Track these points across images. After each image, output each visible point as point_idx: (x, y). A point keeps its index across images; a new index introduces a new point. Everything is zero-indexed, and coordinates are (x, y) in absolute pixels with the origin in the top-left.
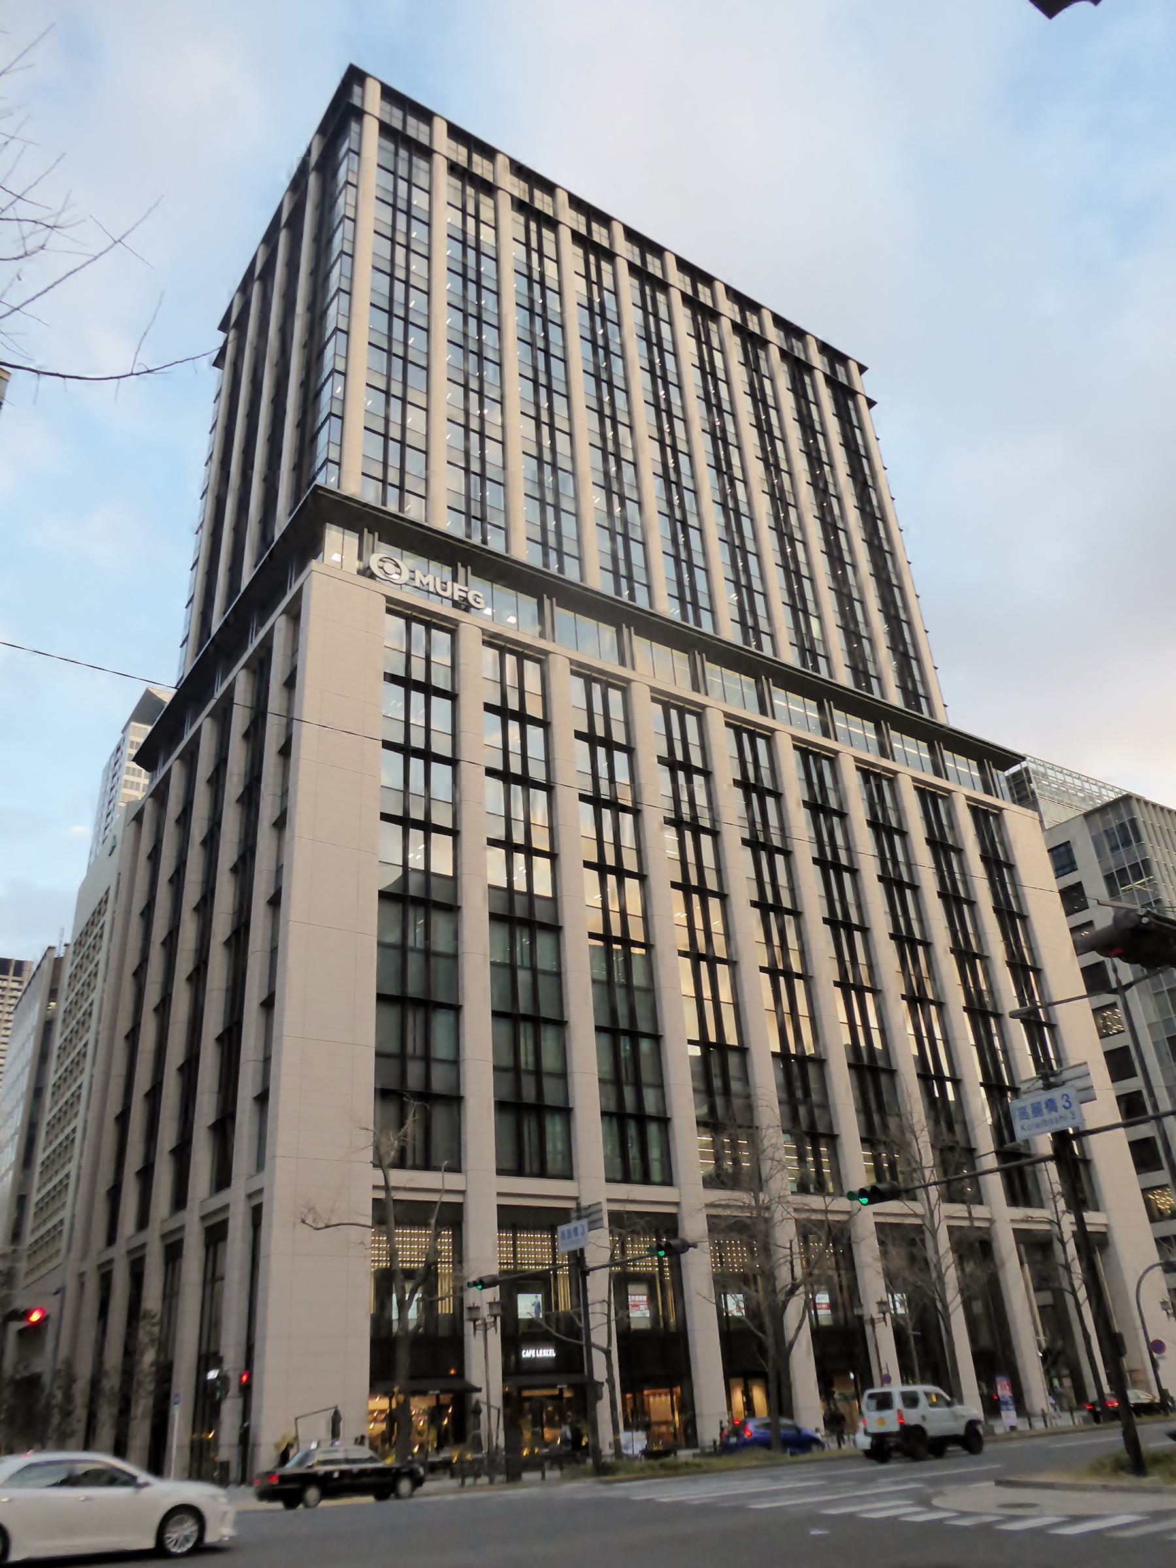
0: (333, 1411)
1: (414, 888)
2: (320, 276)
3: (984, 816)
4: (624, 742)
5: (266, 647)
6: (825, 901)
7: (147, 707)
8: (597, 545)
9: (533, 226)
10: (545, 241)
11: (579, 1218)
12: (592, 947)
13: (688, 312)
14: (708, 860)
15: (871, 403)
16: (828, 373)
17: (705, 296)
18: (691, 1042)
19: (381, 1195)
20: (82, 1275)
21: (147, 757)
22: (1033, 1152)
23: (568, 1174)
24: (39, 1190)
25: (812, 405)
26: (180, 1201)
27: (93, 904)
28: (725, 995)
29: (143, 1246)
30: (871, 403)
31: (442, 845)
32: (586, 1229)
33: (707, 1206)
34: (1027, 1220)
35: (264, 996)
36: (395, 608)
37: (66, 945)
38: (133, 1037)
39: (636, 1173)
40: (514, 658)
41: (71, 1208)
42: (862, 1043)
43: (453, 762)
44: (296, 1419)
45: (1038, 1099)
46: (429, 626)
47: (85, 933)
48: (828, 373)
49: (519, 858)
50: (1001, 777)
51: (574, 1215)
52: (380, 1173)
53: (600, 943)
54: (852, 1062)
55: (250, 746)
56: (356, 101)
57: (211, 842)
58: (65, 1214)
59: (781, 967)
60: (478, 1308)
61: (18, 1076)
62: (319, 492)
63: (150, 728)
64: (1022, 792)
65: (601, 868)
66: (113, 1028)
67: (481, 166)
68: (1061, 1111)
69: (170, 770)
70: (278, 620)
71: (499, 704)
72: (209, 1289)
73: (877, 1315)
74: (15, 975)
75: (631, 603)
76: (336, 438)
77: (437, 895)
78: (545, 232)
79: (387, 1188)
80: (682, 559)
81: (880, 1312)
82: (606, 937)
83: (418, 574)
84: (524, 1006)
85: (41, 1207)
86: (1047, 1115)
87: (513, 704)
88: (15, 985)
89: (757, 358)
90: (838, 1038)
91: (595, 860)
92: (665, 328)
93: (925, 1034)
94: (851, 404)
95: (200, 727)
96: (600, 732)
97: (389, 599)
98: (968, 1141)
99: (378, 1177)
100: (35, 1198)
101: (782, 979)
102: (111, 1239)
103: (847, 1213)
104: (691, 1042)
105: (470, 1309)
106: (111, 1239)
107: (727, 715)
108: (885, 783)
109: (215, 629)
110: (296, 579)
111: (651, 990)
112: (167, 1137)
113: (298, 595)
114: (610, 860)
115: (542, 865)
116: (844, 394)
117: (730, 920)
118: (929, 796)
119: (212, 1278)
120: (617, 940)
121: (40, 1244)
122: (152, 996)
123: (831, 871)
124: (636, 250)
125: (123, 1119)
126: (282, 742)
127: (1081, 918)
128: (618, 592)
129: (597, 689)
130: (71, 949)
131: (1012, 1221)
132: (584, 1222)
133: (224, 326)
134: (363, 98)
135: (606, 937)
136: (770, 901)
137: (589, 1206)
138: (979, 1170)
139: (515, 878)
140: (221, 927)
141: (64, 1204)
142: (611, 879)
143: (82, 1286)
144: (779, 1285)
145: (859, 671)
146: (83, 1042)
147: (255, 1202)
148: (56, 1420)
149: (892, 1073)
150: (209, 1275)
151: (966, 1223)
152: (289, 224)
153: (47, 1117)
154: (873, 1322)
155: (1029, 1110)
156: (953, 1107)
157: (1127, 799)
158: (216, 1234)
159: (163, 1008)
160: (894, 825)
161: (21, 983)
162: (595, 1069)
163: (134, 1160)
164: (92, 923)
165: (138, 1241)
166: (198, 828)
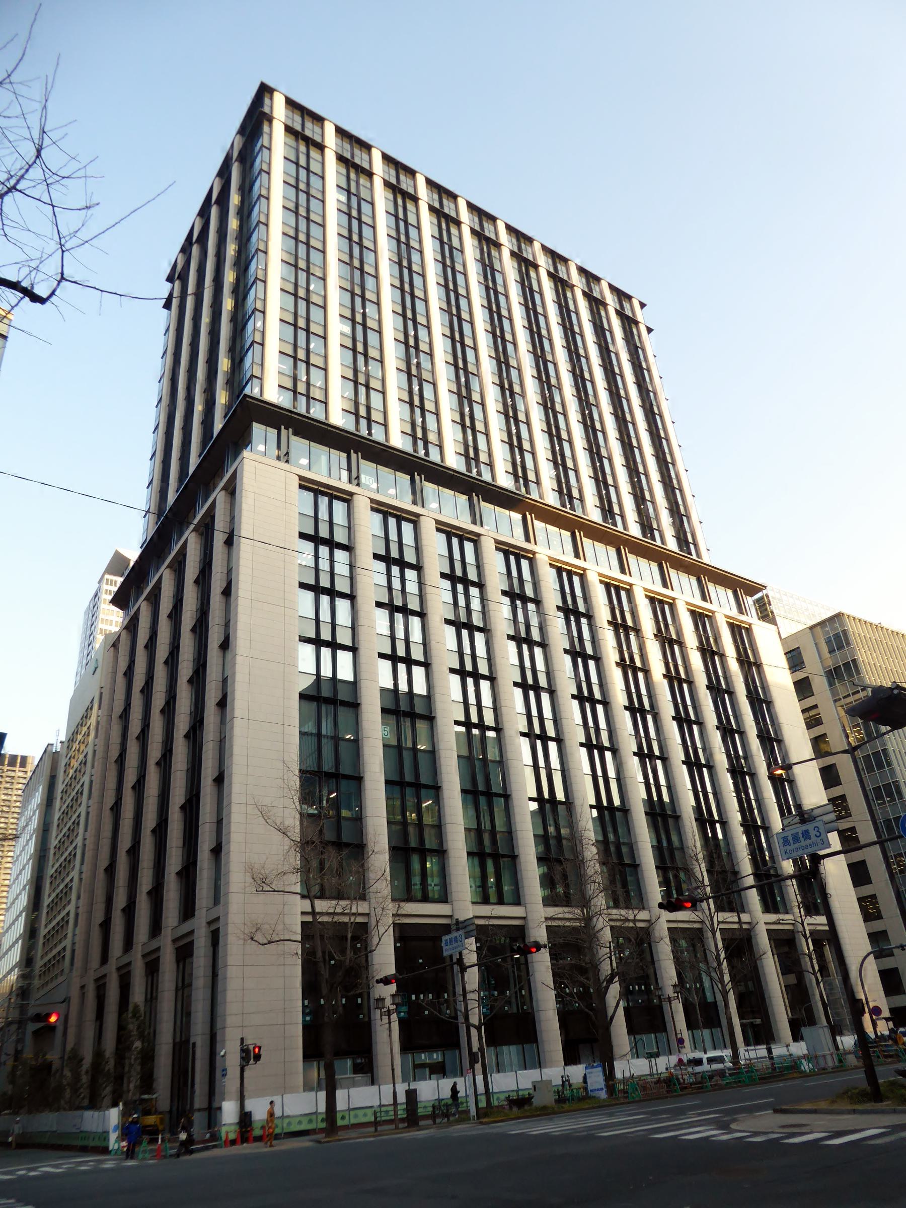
1: (326, 692)
2: (244, 237)
3: (738, 631)
4: (476, 580)
5: (210, 515)
6: (625, 693)
7: (117, 563)
8: (452, 436)
9: (353, 176)
10: (409, 214)
11: (458, 930)
12: (457, 733)
16: (618, 308)
18: (531, 799)
19: (309, 919)
20: (83, 987)
21: (120, 600)
22: (780, 873)
23: (444, 898)
24: (46, 926)
26: (156, 928)
27: (81, 711)
28: (555, 763)
29: (129, 964)
31: (345, 659)
32: (463, 937)
33: (546, 919)
34: (777, 923)
35: (216, 774)
36: (306, 484)
37: (61, 742)
38: (116, 808)
39: (493, 897)
40: (394, 520)
41: (73, 937)
42: (655, 799)
43: (351, 597)
45: (797, 830)
46: (332, 497)
47: (76, 733)
48: (618, 308)
49: (402, 667)
50: (749, 601)
51: (454, 927)
52: (307, 902)
53: (462, 729)
54: (648, 811)
55: (200, 589)
56: (266, 109)
57: (172, 660)
58: (67, 943)
60: (383, 999)
61: (28, 841)
62: (248, 399)
63: (120, 580)
64: (765, 613)
65: (461, 672)
66: (101, 803)
68: (814, 838)
69: (139, 609)
70: (219, 496)
71: (384, 554)
72: (180, 993)
73: (672, 995)
74: (20, 767)
76: (258, 360)
77: (343, 695)
79: (313, 913)
80: (515, 444)
81: (674, 993)
82: (467, 724)
84: (408, 778)
85: (48, 939)
86: (804, 843)
87: (395, 554)
88: (21, 774)
90: (639, 793)
91: (458, 667)
93: (700, 789)
95: (186, 541)
97: (301, 478)
98: (733, 866)
99: (306, 905)
100: (43, 932)
101: (596, 752)
102: (104, 959)
103: (648, 921)
104: (531, 799)
105: (377, 1000)
106: (104, 959)
108: (666, 607)
109: (192, 469)
110: (231, 465)
111: (502, 763)
112: (145, 881)
113: (234, 476)
114: (469, 667)
115: (418, 673)
116: (629, 322)
119: (184, 986)
120: (476, 726)
121: (48, 967)
122: (130, 777)
125: (110, 870)
126: (224, 585)
127: (809, 702)
129: (455, 541)
130: (66, 745)
131: (766, 923)
132: (461, 932)
133: (170, 279)
134: (272, 107)
135: (467, 724)
136: (586, 694)
137: (465, 921)
138: (741, 887)
139: (399, 682)
140: (182, 724)
141: (65, 936)
142: (470, 681)
143: (83, 995)
144: (602, 978)
146: (77, 814)
147: (213, 927)
148: (68, 1093)
149: (677, 818)
150: (149, 996)
151: (736, 926)
152: (218, 202)
153: (51, 871)
154: (669, 1000)
155: (790, 838)
156: (722, 844)
158: (184, 952)
159: (139, 786)
160: (674, 637)
161: (26, 772)
163: (120, 900)
164: (72, 740)
165: (125, 960)
166: (162, 651)
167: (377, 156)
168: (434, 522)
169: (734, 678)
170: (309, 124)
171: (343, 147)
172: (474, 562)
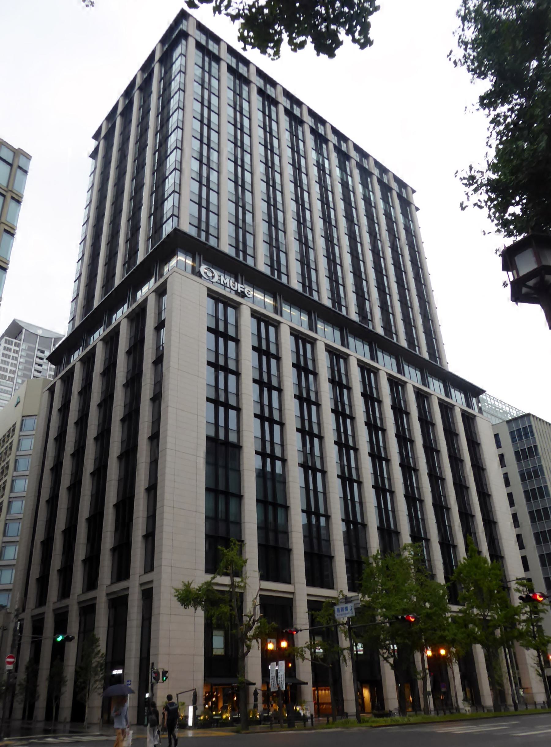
0: (192, 692)
9: (207, 59)
13: (313, 137)
14: (275, 404)
15: (417, 209)
17: (321, 130)
25: (300, 141)
30: (417, 209)
44: (177, 695)
59: (310, 464)
67: (213, 47)
75: (244, 262)
78: (213, 64)
83: (222, 278)
84: (221, 487)
89: (321, 147)
92: (274, 125)
94: (369, 179)
96: (221, 328)
97: (209, 289)
107: (291, 328)
117: (324, 450)
118: (395, 383)
123: (341, 417)
124: (288, 102)
128: (199, 235)
136: (307, 429)
145: (387, 326)
157: (528, 415)
162: (203, 510)
167: (253, 70)
168: (289, 328)
169: (357, 407)
170: (211, 42)
171: (201, 37)
172: (274, 341)
